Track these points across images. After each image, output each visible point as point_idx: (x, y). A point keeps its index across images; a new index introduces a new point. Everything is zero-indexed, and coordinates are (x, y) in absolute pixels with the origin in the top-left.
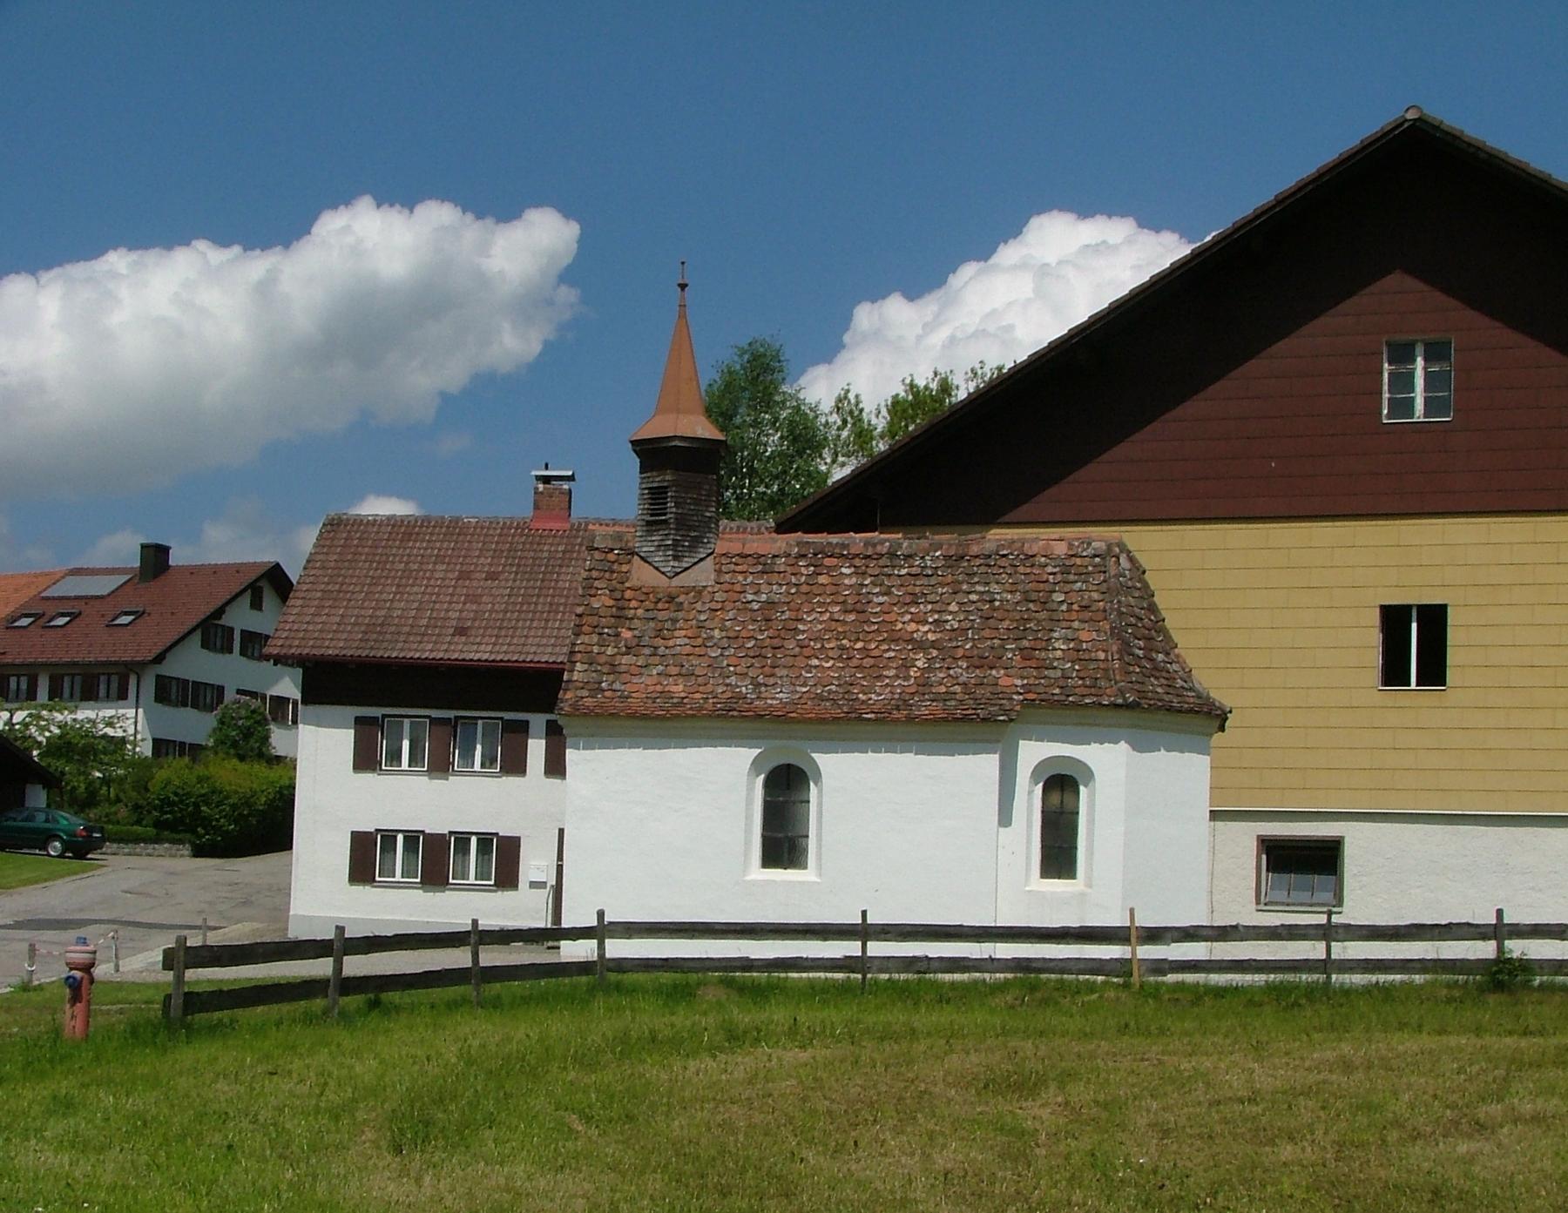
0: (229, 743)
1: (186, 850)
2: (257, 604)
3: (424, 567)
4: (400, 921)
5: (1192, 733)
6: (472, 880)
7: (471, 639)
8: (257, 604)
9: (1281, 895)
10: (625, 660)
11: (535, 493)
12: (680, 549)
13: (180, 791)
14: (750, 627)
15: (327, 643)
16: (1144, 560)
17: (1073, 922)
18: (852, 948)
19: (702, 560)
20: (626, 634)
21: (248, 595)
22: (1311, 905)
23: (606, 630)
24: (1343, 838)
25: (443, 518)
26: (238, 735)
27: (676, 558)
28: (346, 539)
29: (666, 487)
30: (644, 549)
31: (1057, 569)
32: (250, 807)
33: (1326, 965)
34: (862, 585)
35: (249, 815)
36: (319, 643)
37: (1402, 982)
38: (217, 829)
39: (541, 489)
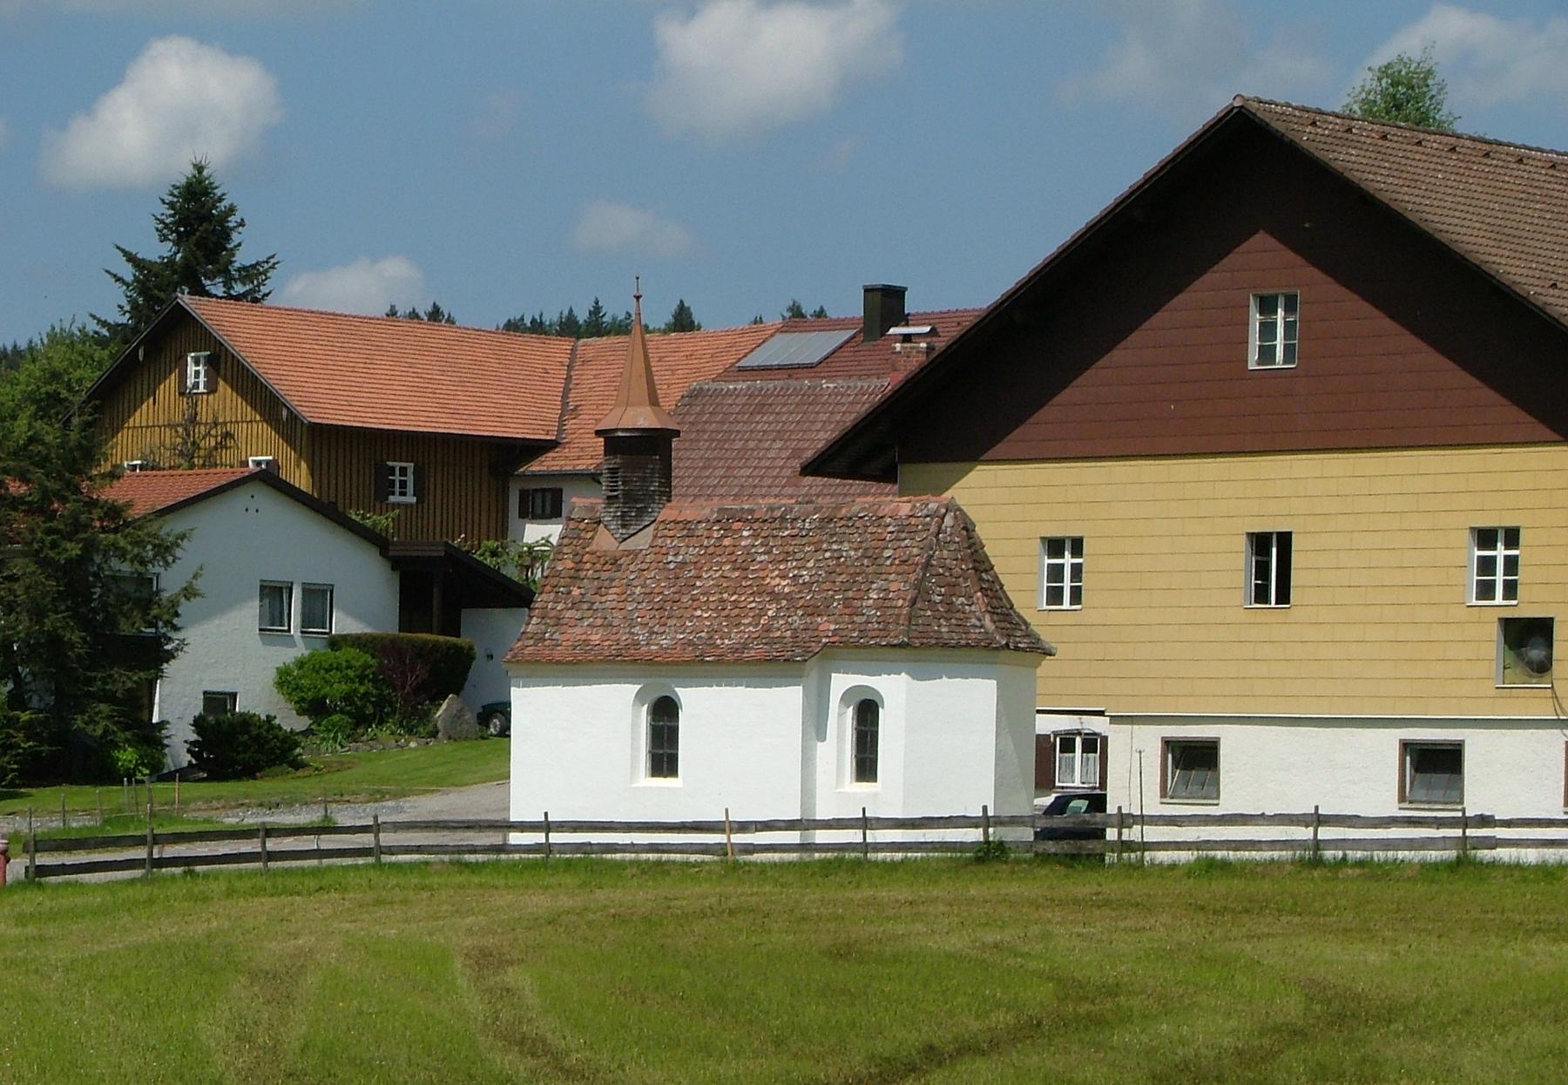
5: (973, 662)
9: (1421, 794)
10: (568, 614)
14: (663, 584)
16: (973, 514)
17: (689, 818)
18: (539, 838)
20: (576, 592)
22: (1429, 803)
24: (1219, 738)
27: (624, 526)
33: (865, 847)
34: (754, 546)
37: (922, 858)
39: (898, 349)
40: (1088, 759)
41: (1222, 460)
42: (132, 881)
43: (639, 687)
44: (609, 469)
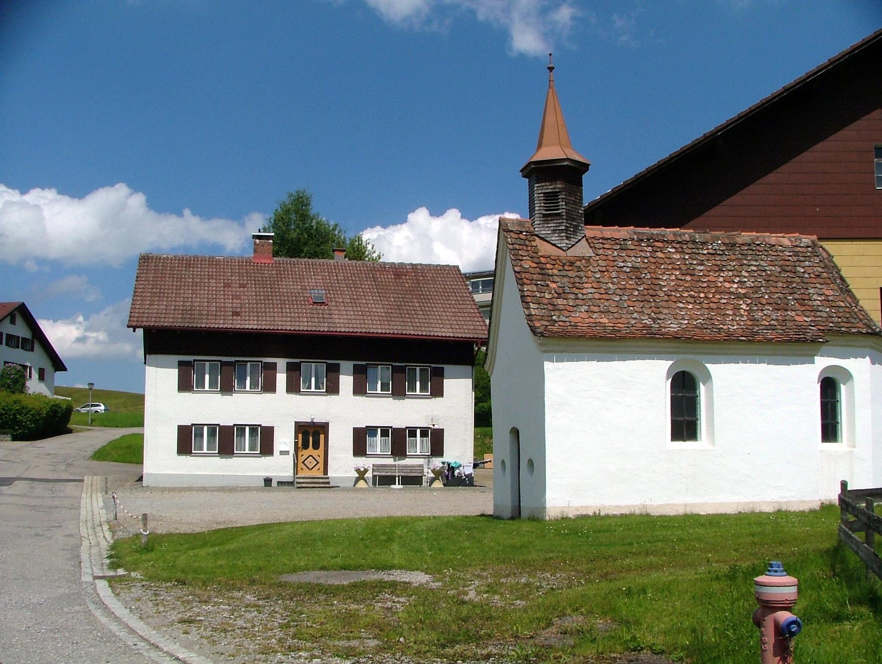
0: (6, 386)
1: (9, 437)
2: (13, 322)
3: (203, 280)
4: (208, 475)
6: (247, 451)
7: (243, 318)
8: (13, 322)
11: (255, 244)
12: (569, 232)
13: (6, 408)
15: (163, 320)
19: (580, 240)
21: (9, 318)
23: (539, 282)
25: (204, 257)
26: (11, 382)
27: (568, 238)
28: (155, 266)
29: (558, 192)
30: (544, 232)
31: (791, 254)
32: (39, 415)
35: (39, 419)
36: (158, 320)
38: (26, 427)
39: (258, 242)
40: (423, 440)
41: (856, 243)
42: (294, 570)
43: (671, 362)
44: (544, 193)
